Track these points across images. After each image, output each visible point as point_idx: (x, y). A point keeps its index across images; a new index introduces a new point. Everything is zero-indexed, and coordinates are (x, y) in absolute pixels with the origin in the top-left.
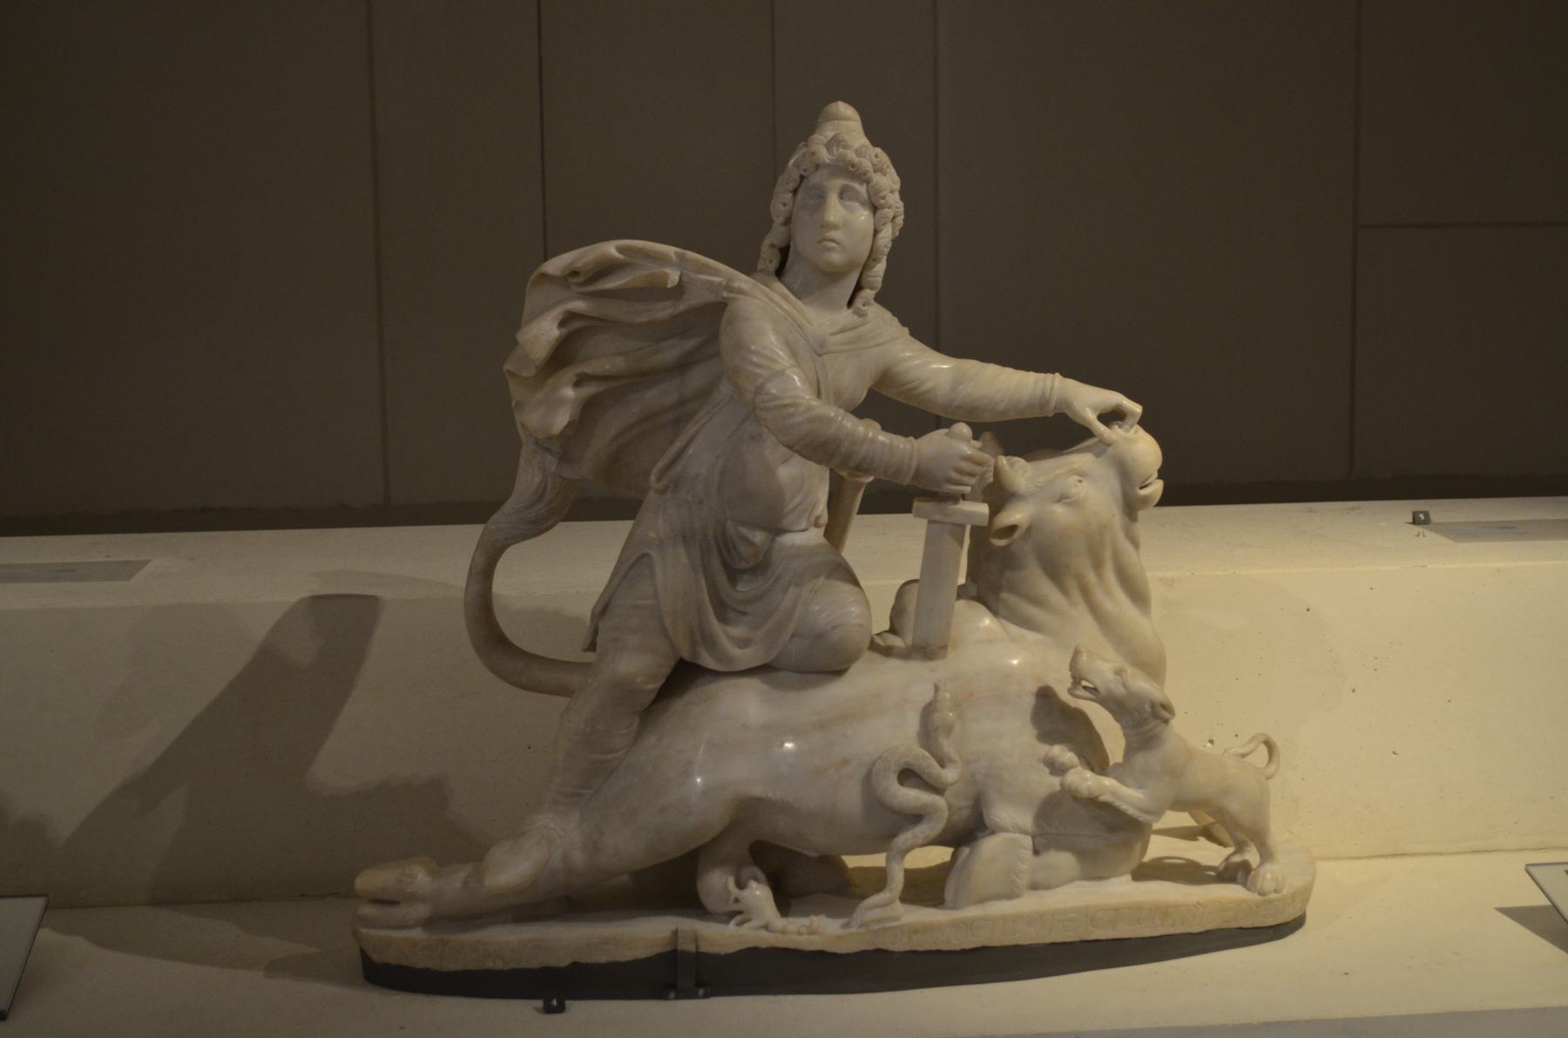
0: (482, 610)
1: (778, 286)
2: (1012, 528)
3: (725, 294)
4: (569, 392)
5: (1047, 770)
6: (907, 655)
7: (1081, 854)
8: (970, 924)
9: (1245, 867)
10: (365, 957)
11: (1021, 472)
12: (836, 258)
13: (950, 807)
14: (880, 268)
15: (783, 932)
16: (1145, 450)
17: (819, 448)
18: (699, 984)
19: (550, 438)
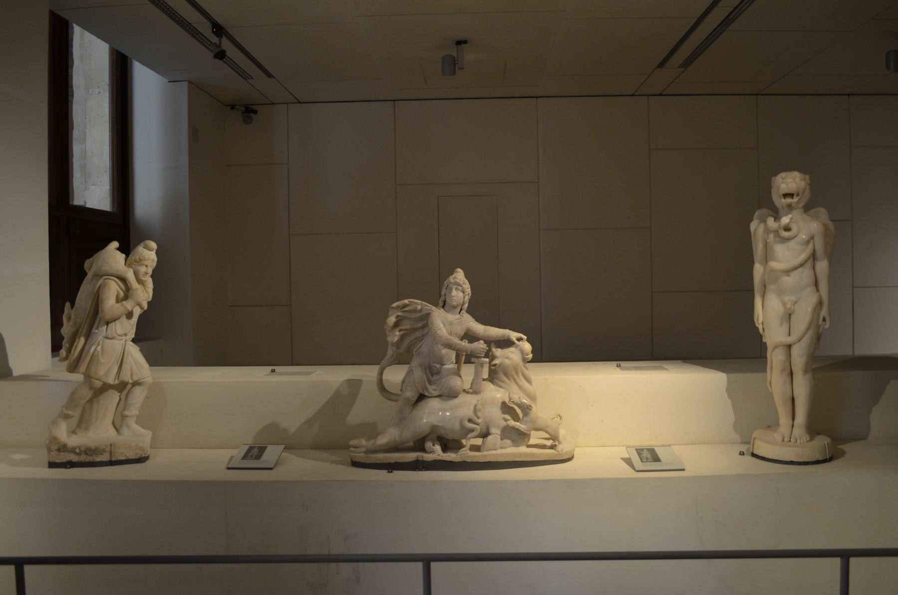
0: (380, 382)
1: (442, 310)
2: (496, 364)
3: (430, 311)
4: (398, 333)
5: (503, 421)
6: (472, 393)
7: (513, 441)
8: (485, 456)
9: (556, 445)
10: (352, 460)
11: (498, 352)
12: (455, 303)
13: (481, 428)
14: (466, 305)
15: (443, 456)
16: (527, 347)
17: (449, 346)
18: (423, 468)
19: (394, 343)
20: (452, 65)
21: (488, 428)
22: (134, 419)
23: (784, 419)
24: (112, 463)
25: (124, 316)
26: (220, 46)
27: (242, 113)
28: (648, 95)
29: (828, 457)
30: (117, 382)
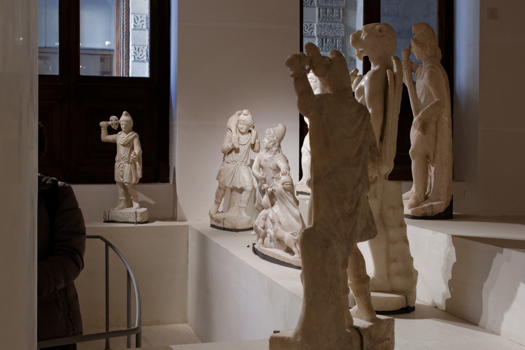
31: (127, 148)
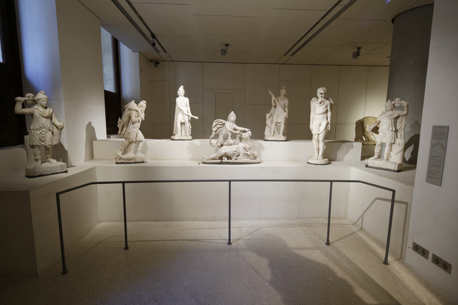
11: (243, 134)
14: (235, 121)
16: (250, 133)
17: (230, 132)
20: (224, 52)
21: (239, 154)
22: (140, 151)
23: (316, 154)
24: (135, 163)
25: (138, 122)
26: (154, 42)
27: (155, 63)
28: (369, 66)
29: (327, 163)
30: (136, 140)
31: (48, 119)
